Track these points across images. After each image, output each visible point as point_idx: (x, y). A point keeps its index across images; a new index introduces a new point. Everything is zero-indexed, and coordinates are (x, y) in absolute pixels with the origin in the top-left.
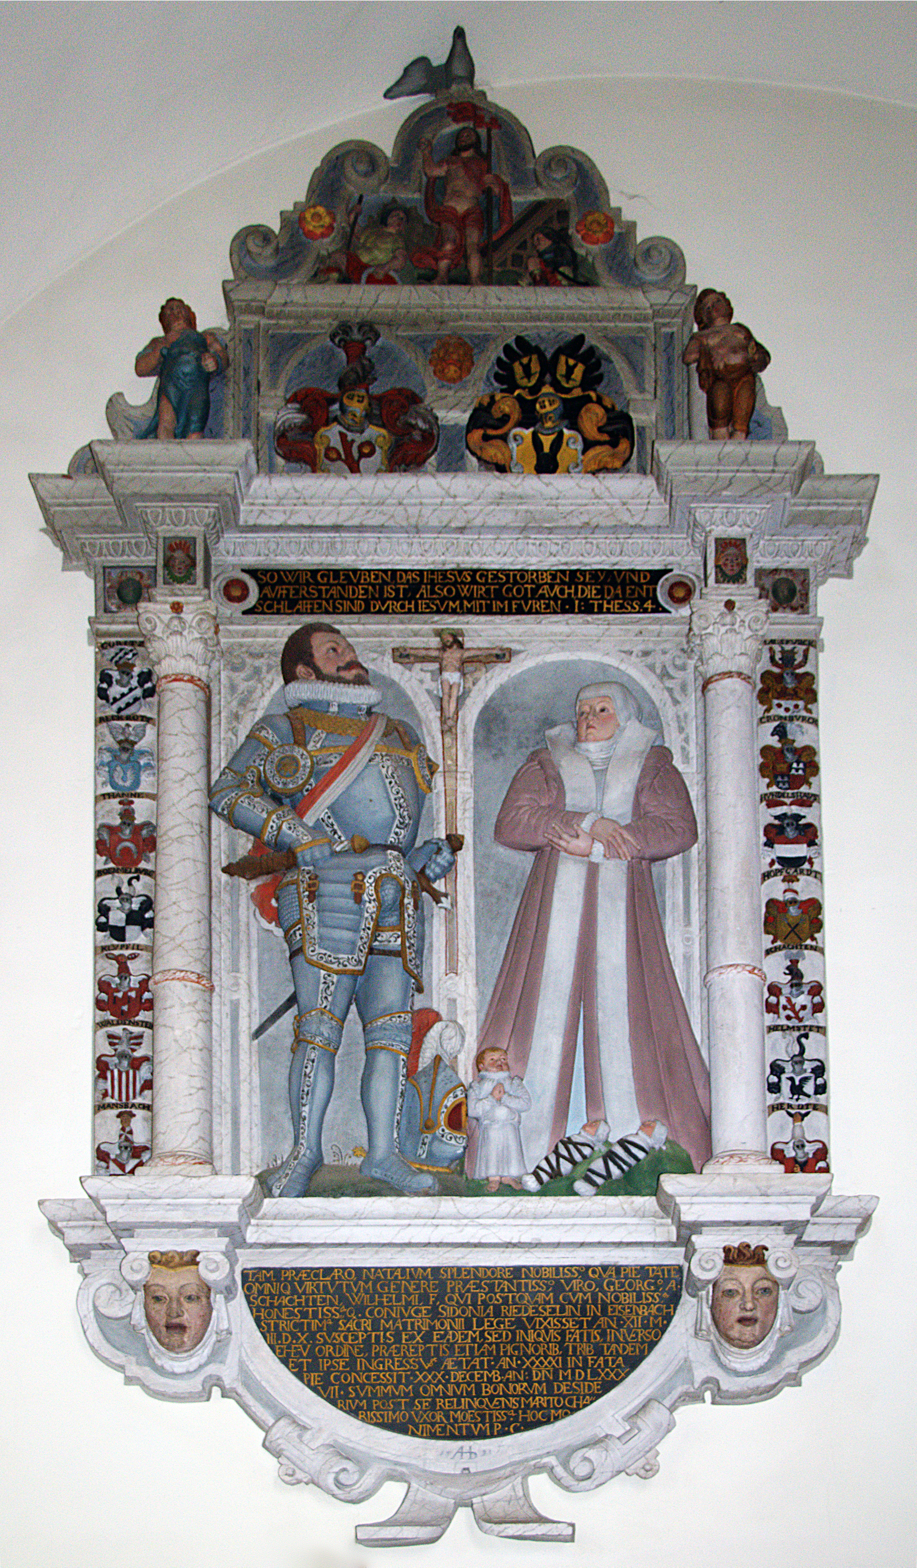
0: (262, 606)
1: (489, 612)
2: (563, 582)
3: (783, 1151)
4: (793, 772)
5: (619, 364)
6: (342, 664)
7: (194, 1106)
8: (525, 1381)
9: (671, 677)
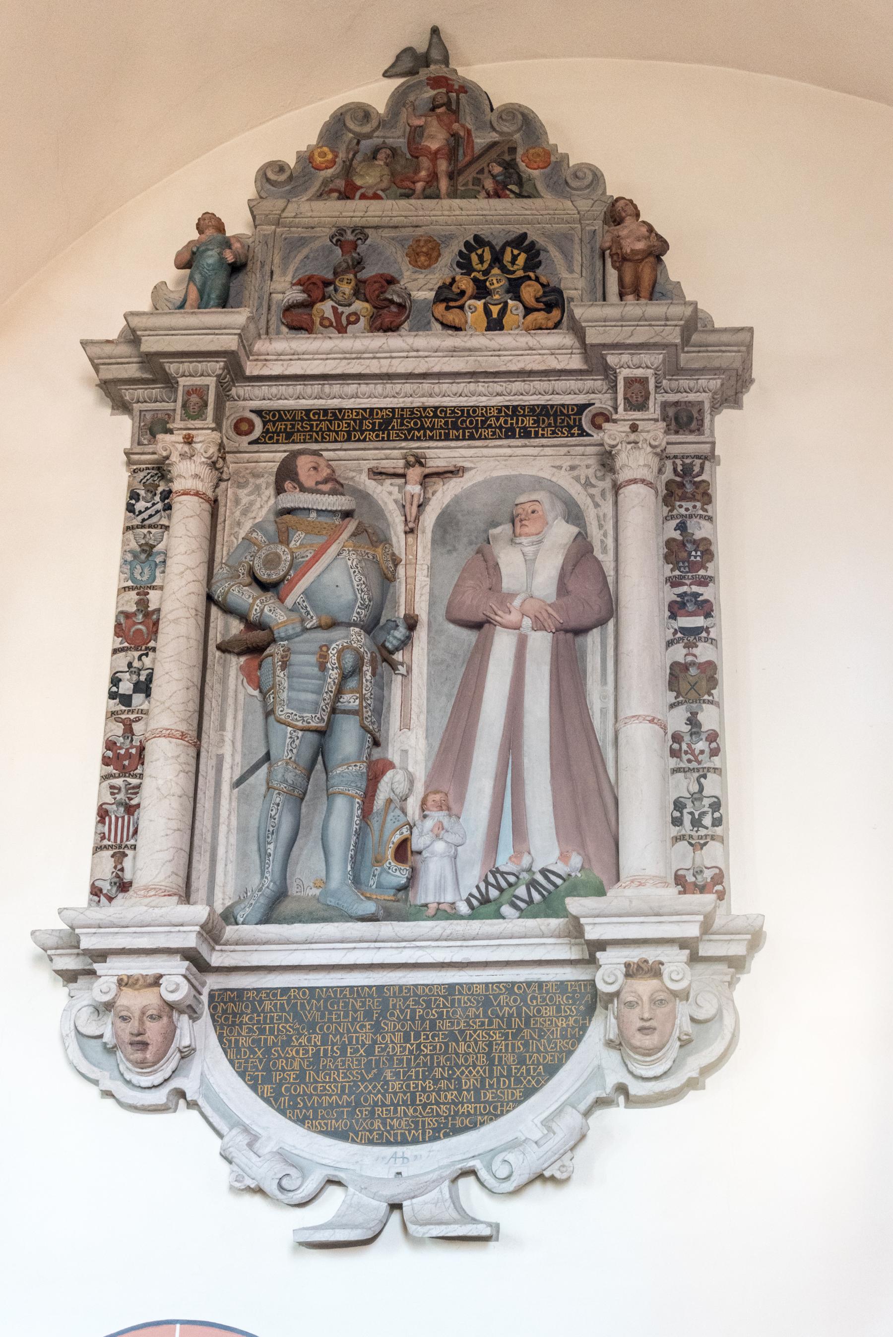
0: (264, 437)
1: (447, 438)
2: (507, 415)
3: (685, 876)
4: (692, 558)
5: (554, 253)
6: (319, 479)
7: (170, 845)
8: (455, 1089)
9: (594, 486)
